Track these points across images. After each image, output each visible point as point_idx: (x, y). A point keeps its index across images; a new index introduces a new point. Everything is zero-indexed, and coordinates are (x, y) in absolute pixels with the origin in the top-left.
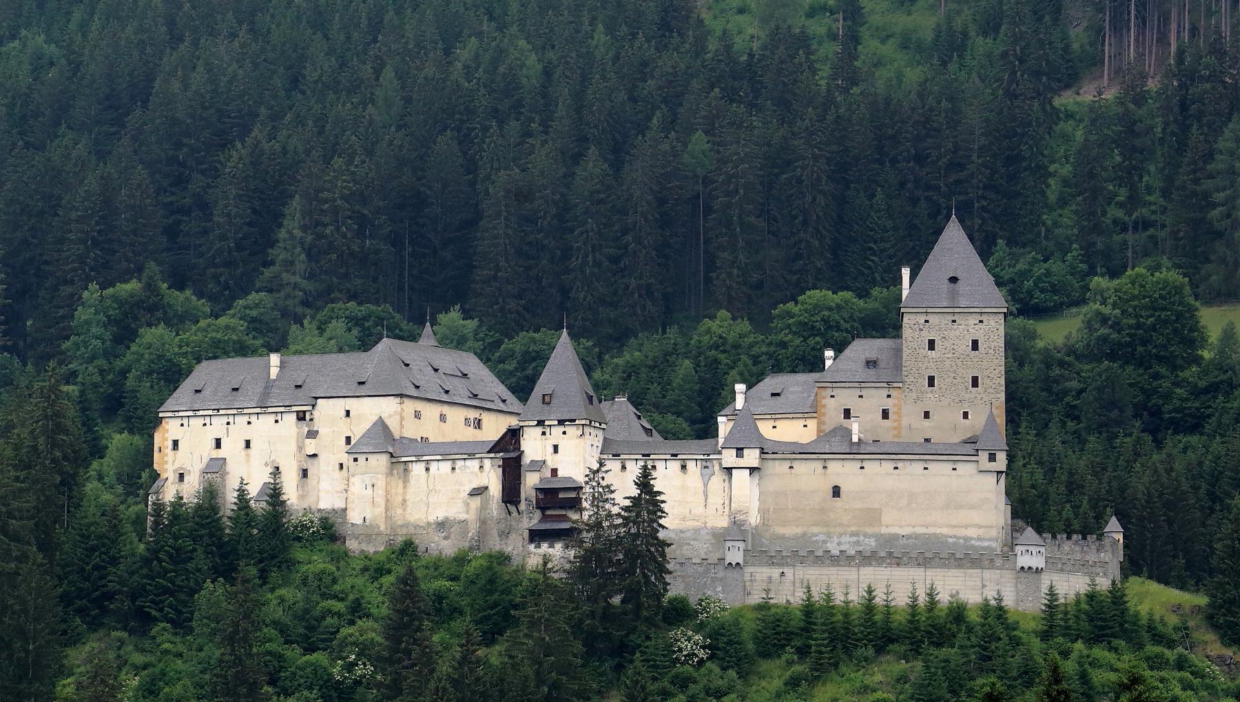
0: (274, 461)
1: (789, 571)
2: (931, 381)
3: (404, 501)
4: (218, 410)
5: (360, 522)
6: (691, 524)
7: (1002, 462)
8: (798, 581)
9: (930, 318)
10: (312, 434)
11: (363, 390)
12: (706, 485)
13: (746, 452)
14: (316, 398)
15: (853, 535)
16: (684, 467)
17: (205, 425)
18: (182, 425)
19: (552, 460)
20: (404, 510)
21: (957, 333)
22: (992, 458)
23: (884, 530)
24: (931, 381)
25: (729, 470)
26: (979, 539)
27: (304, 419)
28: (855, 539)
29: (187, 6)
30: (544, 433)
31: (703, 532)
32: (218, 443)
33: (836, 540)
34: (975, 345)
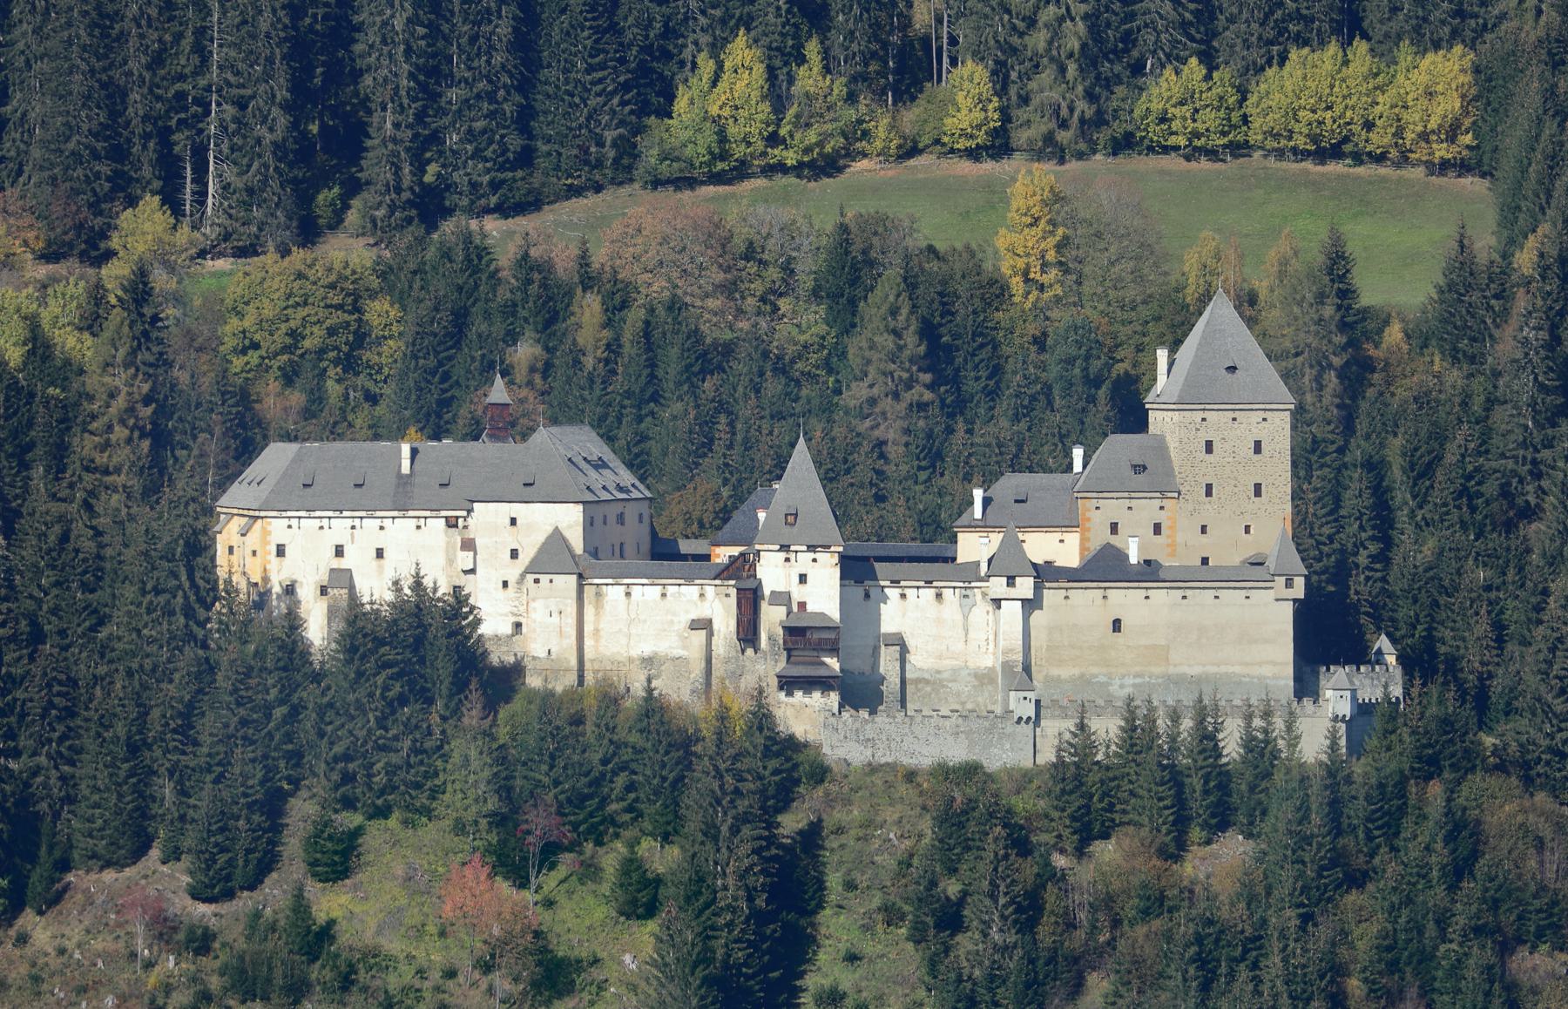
2: (1209, 490)
5: (542, 654)
7: (1299, 590)
9: (1207, 414)
10: (468, 545)
12: (966, 617)
13: (1018, 580)
16: (939, 596)
19: (798, 594)
20: (597, 641)
22: (1289, 584)
23: (1172, 670)
24: (1209, 490)
25: (997, 602)
27: (456, 526)
30: (787, 560)
31: (964, 673)
32: (339, 551)
33: (1118, 682)
34: (1258, 448)
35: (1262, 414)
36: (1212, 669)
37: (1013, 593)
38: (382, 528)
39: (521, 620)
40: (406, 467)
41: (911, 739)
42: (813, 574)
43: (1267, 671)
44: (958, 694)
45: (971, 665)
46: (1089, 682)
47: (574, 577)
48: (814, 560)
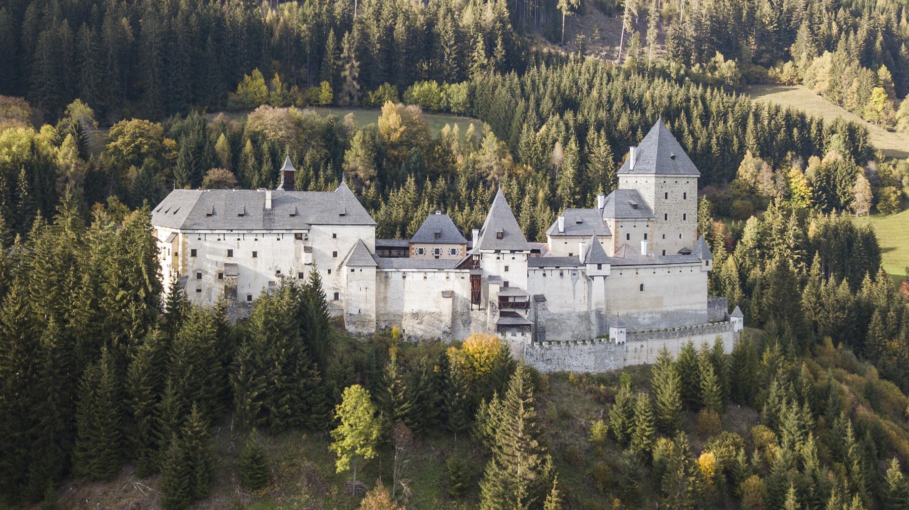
0: (276, 267)
1: (644, 343)
3: (385, 297)
4: (232, 230)
5: (356, 312)
6: (566, 310)
8: (649, 350)
9: (666, 180)
11: (343, 220)
12: (574, 285)
13: (603, 266)
14: (311, 225)
15: (650, 313)
16: (561, 274)
17: (219, 240)
18: (199, 239)
19: (505, 276)
20: (386, 304)
21: (678, 189)
23: (665, 309)
26: (701, 310)
28: (651, 315)
29: (5, 463)
30: (498, 258)
31: (574, 315)
32: (230, 253)
33: (642, 317)
35: (687, 180)
36: (678, 308)
37: (601, 272)
38: (256, 240)
39: (693, 253)
40: (268, 205)
41: (568, 358)
42: (512, 265)
43: (698, 307)
44: (571, 326)
45: (577, 310)
46: (630, 318)
47: (374, 270)
48: (513, 258)
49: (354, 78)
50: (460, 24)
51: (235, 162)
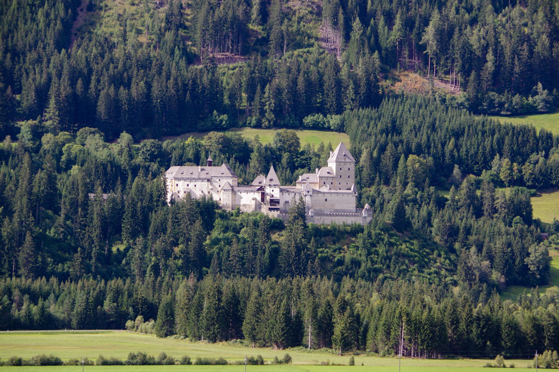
11: (223, 175)
19: (272, 193)
34: (349, 169)
43: (351, 209)
49: (271, 110)
50: (378, 63)
51: (214, 68)
